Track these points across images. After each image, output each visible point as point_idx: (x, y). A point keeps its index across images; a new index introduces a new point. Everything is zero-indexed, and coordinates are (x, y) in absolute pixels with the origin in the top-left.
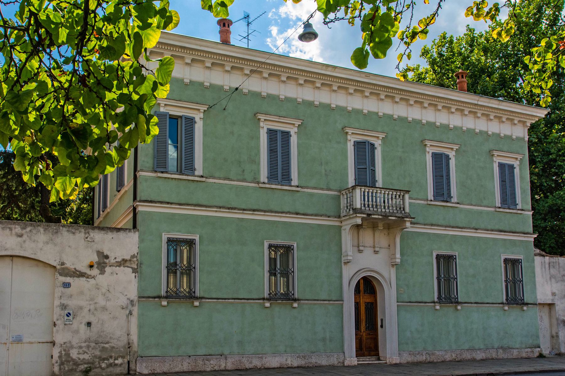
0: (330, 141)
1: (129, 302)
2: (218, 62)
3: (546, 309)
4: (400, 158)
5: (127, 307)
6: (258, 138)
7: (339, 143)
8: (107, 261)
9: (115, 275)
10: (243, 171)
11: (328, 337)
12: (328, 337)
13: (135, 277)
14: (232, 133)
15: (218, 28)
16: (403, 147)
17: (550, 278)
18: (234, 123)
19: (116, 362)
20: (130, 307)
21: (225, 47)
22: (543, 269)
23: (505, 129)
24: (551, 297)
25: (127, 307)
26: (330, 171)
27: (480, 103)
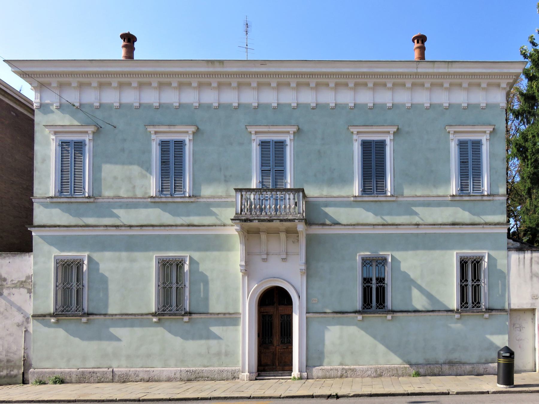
0: (231, 144)
1: (24, 320)
2: (417, 82)
3: (310, 311)
4: (319, 152)
5: (22, 324)
6: (150, 152)
7: (241, 144)
8: (5, 283)
9: (12, 295)
10: (134, 187)
11: (223, 351)
12: (223, 351)
13: (30, 296)
14: (123, 150)
15: (122, 42)
16: (323, 139)
17: (531, 277)
18: (125, 140)
19: (12, 373)
20: (25, 323)
21: (130, 63)
22: (522, 266)
23: (479, 98)
24: (531, 301)
25: (22, 324)
26: (231, 176)
27: (420, 70)
